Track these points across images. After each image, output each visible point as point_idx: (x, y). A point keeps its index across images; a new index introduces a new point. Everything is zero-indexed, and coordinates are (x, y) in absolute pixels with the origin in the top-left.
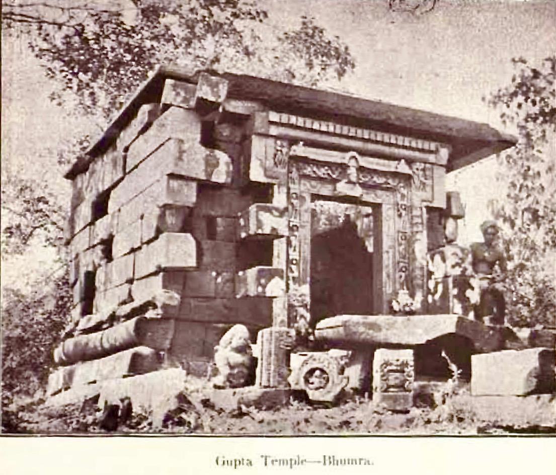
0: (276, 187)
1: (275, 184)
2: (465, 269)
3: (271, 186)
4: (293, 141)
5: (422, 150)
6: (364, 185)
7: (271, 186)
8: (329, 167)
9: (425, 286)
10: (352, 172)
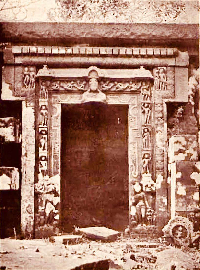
0: (24, 103)
1: (23, 101)
2: (190, 155)
3: (20, 102)
4: (39, 66)
5: (160, 57)
6: (106, 92)
7: (20, 102)
8: (74, 81)
9: (165, 168)
10: (94, 84)
